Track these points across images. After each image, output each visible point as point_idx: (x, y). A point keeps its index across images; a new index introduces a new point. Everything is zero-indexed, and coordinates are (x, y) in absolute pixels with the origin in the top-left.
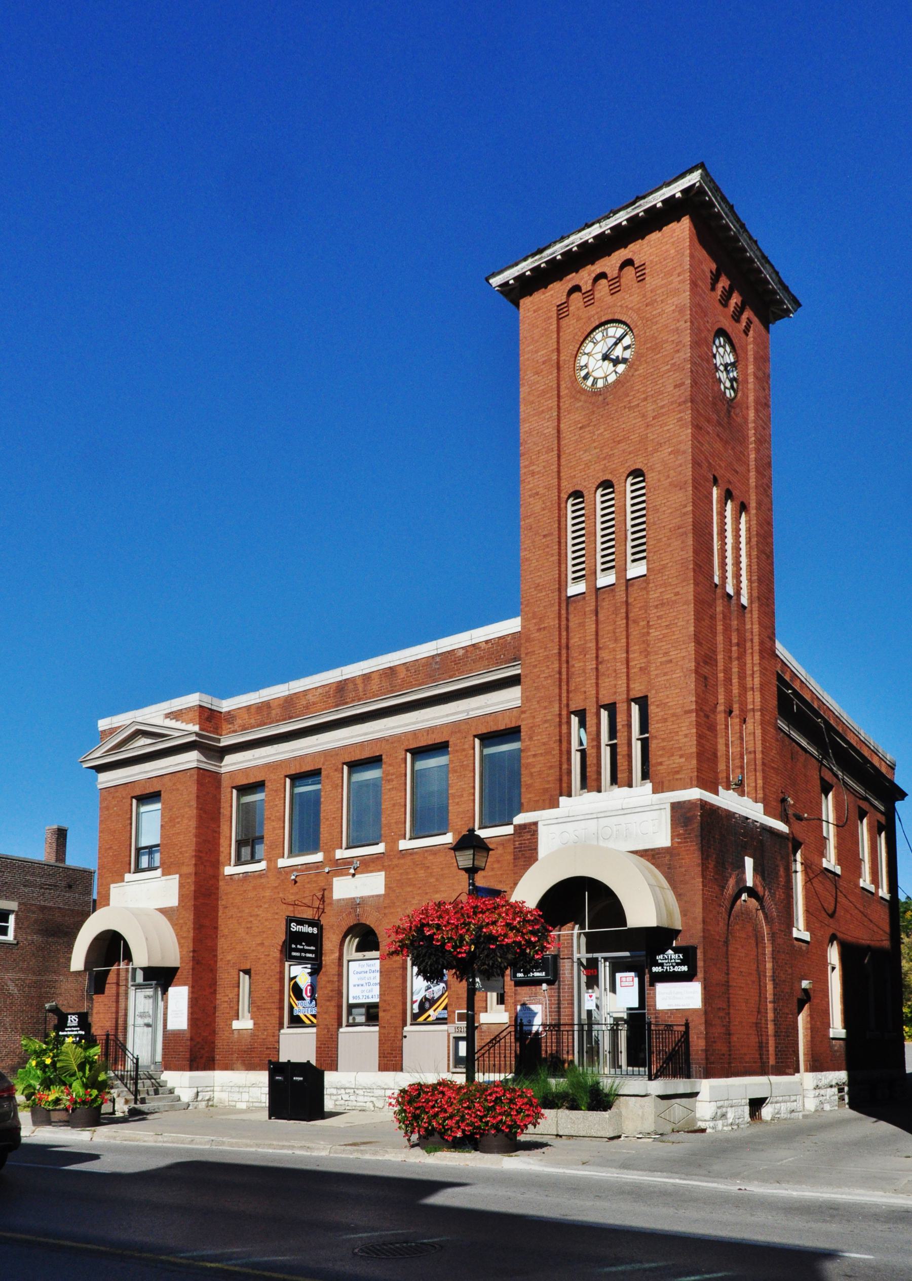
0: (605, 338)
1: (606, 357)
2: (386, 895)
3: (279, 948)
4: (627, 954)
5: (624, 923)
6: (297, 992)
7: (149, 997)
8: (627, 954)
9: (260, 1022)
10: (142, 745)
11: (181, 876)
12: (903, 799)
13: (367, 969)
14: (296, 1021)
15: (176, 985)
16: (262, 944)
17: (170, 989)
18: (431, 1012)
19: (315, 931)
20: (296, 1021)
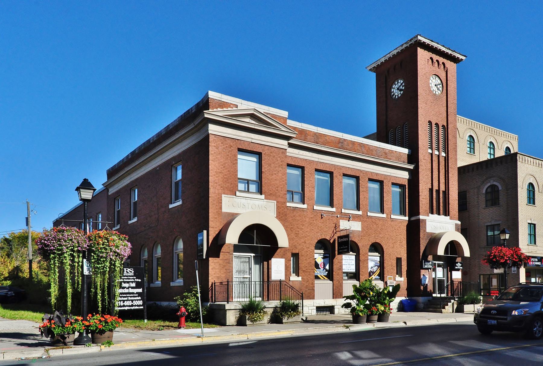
0: (398, 83)
1: (398, 89)
2: (362, 231)
3: (369, 247)
4: (197, 271)
5: (339, 253)
6: (317, 266)
7: (245, 262)
8: (197, 271)
9: (305, 277)
10: (248, 122)
11: (277, 202)
12: (87, 180)
13: (348, 258)
14: (317, 277)
15: (276, 258)
16: (305, 242)
17: (273, 259)
18: (373, 276)
19: (100, 228)
20: (317, 277)
